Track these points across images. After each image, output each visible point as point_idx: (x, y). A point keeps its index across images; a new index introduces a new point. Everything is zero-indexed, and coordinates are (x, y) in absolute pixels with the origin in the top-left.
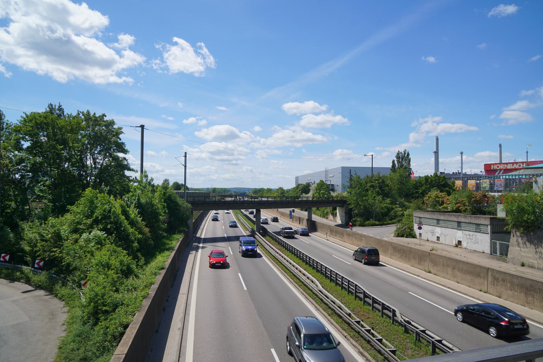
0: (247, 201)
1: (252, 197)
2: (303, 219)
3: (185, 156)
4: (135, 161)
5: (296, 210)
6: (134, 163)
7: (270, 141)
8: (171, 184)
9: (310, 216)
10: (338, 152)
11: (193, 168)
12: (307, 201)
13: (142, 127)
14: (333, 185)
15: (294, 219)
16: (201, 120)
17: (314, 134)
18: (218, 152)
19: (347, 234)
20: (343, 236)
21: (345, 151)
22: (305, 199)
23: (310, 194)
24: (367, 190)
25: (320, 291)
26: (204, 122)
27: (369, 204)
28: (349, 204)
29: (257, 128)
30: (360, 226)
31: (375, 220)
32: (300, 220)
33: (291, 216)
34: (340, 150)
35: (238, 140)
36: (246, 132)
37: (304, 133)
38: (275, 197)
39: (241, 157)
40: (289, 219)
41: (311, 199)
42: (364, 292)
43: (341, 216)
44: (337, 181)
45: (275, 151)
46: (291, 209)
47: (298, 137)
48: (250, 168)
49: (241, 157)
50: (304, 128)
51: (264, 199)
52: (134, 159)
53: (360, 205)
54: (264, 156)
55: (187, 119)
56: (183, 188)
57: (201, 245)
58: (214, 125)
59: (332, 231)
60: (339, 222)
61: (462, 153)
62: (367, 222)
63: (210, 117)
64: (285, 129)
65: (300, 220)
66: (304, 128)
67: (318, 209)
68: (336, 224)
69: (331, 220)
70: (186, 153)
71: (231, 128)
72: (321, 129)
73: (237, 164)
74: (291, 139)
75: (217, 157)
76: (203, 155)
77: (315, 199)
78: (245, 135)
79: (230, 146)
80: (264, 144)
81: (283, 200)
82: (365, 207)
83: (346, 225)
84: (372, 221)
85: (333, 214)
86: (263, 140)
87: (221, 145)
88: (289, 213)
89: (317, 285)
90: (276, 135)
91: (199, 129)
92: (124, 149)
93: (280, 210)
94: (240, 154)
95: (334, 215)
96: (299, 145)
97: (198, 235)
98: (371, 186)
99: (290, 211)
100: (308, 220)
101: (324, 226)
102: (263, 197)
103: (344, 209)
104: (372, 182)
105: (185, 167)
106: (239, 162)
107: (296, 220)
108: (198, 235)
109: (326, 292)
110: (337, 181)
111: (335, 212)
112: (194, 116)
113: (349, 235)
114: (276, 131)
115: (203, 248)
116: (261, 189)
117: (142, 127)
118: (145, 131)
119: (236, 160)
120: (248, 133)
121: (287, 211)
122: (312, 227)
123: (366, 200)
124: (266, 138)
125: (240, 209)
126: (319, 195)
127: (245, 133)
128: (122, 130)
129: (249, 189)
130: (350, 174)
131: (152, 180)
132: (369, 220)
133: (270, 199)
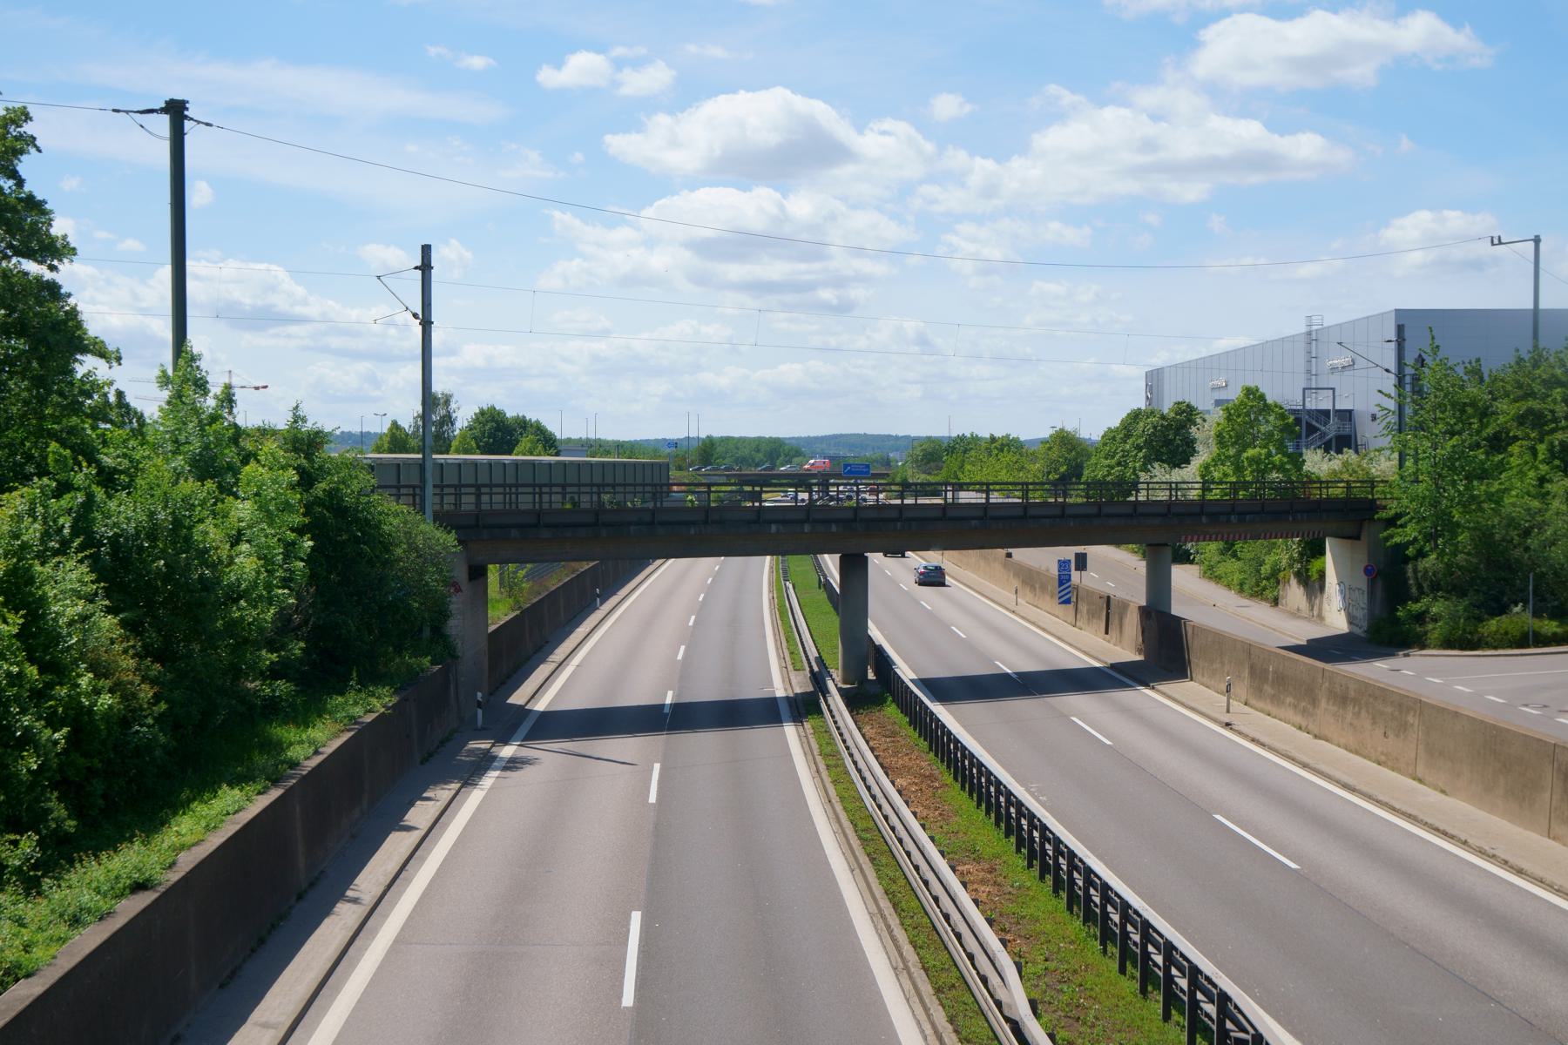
0: (878, 507)
1: (906, 487)
2: (1124, 606)
3: (425, 267)
4: (305, 303)
5: (1095, 552)
6: (299, 310)
7: (1021, 173)
8: (464, 416)
9: (1159, 585)
10: (1413, 226)
11: (605, 333)
12: (1169, 504)
13: (176, 110)
14: (1347, 415)
15: (1083, 608)
16: (638, 64)
17: (1278, 126)
18: (742, 243)
19: (1332, 695)
20: (1314, 702)
21: (1455, 220)
22: (1162, 496)
23: (1190, 473)
24: (1499, 443)
26: (655, 78)
27: (1511, 522)
28: (1391, 522)
29: (947, 106)
30: (1449, 643)
31: (1537, 614)
32: (1108, 611)
33: (1066, 592)
34: (1424, 216)
35: (848, 170)
36: (888, 124)
37: (1217, 122)
38: (1025, 487)
39: (866, 266)
40: (1052, 603)
41: (1194, 494)
43: (1347, 591)
45: (1055, 225)
46: (1069, 552)
47: (1185, 145)
48: (911, 326)
49: (866, 266)
50: (1219, 96)
51: (966, 497)
52: (300, 291)
53: (1454, 528)
54: (996, 254)
55: (559, 65)
56: (525, 442)
57: (507, 751)
58: (713, 92)
59: (1266, 675)
60: (1335, 619)
61: (176, 110)
62: (1493, 624)
63: (692, 48)
64: (1102, 103)
65: (1108, 611)
66: (1219, 96)
67: (1229, 550)
68: (1317, 632)
69: (1296, 614)
70: (426, 250)
71: (801, 104)
72: (1316, 98)
73: (843, 308)
74: (1141, 159)
75: (735, 271)
76: (658, 261)
77: (1215, 494)
78: (884, 144)
79: (802, 206)
80: (989, 191)
82: (1484, 538)
83: (1387, 629)
84: (1520, 617)
85: (1304, 579)
86: (984, 167)
87: (751, 206)
88: (1054, 571)
90: (1054, 139)
91: (632, 115)
92: (53, 240)
94: (859, 251)
95: (1313, 585)
96: (1192, 192)
97: (518, 698)
98: (1521, 420)
99: (1063, 565)
100: (1145, 612)
102: (960, 487)
103: (1360, 555)
104: (1530, 394)
105: (426, 324)
106: (857, 293)
107: (1092, 614)
108: (518, 698)
110: (1367, 392)
111: (1315, 565)
112: (598, 47)
114: (1059, 116)
115: (513, 764)
116: (962, 438)
119: (839, 282)
120: (902, 128)
121: (1044, 559)
122: (1167, 650)
123: (1490, 497)
124: (1002, 157)
126: (1238, 469)
127: (884, 133)
128: (28, 128)
131: (228, 399)
132: (1502, 610)
133: (996, 498)
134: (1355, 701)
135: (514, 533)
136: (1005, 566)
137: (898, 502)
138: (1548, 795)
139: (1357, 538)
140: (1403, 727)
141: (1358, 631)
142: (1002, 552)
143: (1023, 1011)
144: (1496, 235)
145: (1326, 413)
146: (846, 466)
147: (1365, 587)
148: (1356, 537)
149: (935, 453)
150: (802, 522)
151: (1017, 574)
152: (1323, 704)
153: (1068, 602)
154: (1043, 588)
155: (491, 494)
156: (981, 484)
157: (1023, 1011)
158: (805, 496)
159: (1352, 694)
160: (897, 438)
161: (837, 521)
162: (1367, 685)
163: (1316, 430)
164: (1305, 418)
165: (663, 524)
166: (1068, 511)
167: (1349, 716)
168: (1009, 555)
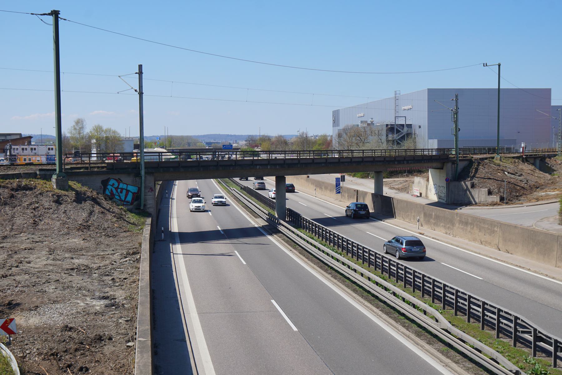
3: (140, 73)
13: (55, 14)
14: (410, 126)
19: (461, 222)
20: (453, 225)
25: (446, 331)
33: (338, 189)
40: (334, 194)
42: (535, 330)
44: (417, 117)
46: (339, 175)
70: (140, 67)
81: (315, 160)
88: (334, 183)
89: (439, 321)
93: (312, 176)
99: (337, 179)
101: (409, 206)
105: (141, 94)
109: (461, 333)
113: (465, 222)
117: (55, 14)
118: (61, 22)
121: (331, 178)
125: (230, 176)
129: (237, 138)
130: (448, 103)
134: (471, 224)
135: (171, 169)
136: (307, 181)
137: (252, 158)
138: (555, 253)
139: (442, 169)
140: (493, 232)
141: (442, 201)
142: (306, 176)
143: (449, 326)
144: (485, 63)
145: (403, 125)
146: (223, 146)
147: (445, 186)
148: (442, 168)
149: (253, 141)
150: (267, 165)
151: (313, 184)
152: (457, 225)
153: (339, 192)
154: (326, 188)
155: (236, 154)
156: (298, 151)
157: (449, 326)
158: (234, 156)
159: (470, 221)
160: (231, 136)
161: (278, 164)
162: (477, 218)
163: (400, 131)
164: (396, 127)
165: (220, 166)
166: (328, 161)
167: (469, 229)
168: (308, 177)
